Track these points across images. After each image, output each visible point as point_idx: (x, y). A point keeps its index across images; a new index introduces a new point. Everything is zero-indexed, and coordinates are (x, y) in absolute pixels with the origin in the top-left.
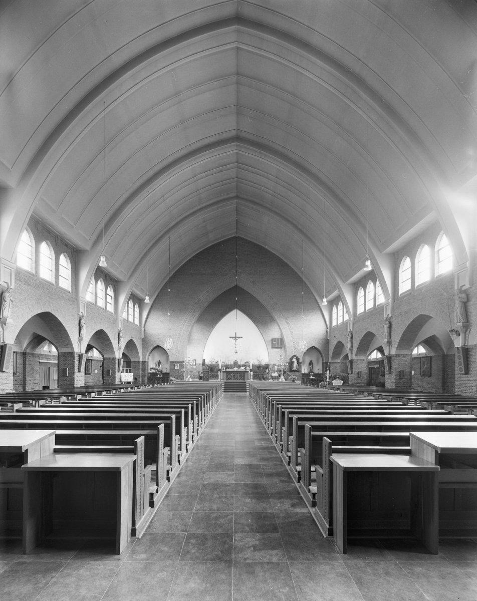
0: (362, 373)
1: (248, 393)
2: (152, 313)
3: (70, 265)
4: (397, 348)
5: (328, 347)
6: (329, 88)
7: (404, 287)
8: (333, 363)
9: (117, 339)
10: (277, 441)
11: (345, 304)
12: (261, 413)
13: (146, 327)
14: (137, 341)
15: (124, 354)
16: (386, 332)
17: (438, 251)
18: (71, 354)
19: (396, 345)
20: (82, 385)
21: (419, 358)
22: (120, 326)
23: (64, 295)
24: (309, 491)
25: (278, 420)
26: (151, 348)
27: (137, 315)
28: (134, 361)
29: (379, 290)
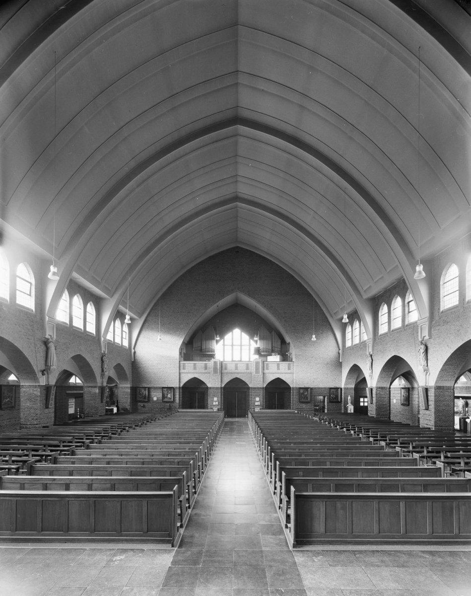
0: (22, 390)
3: (32, 275)
6: (144, 517)
13: (136, 349)
17: (409, 302)
27: (126, 335)
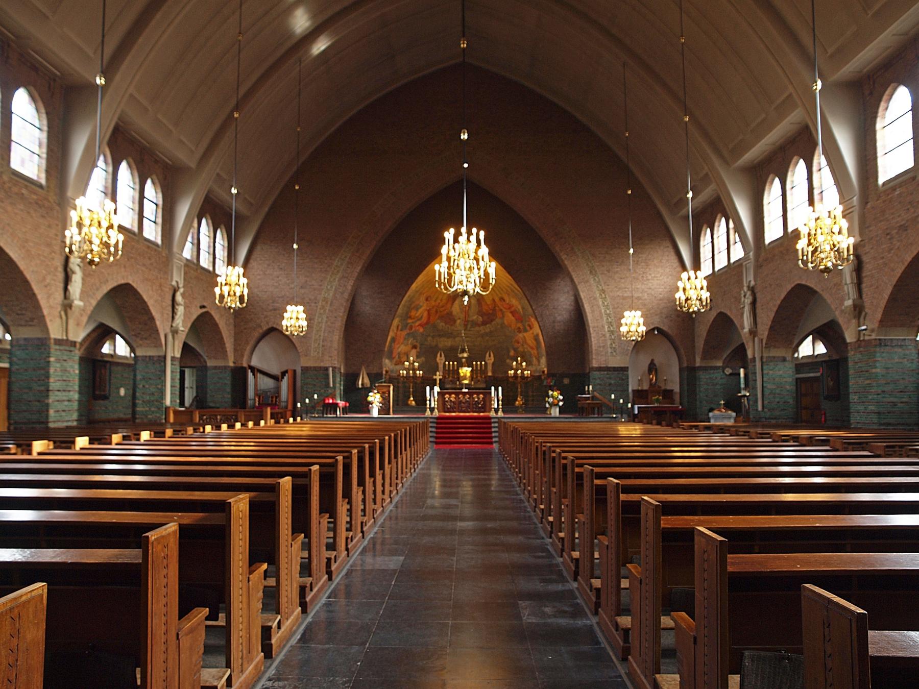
1: (496, 446)
2: (259, 247)
4: (881, 321)
5: (693, 330)
7: (773, 232)
8: (705, 369)
9: (170, 308)
10: (562, 550)
11: (730, 214)
12: (529, 491)
14: (222, 316)
15: (186, 347)
16: (849, 281)
18: (43, 344)
19: (879, 316)
20: (70, 424)
21: (813, 362)
22: (177, 278)
23: (24, 191)
24: (617, 626)
25: (565, 497)
26: (256, 335)
28: (215, 368)
29: (824, 178)
